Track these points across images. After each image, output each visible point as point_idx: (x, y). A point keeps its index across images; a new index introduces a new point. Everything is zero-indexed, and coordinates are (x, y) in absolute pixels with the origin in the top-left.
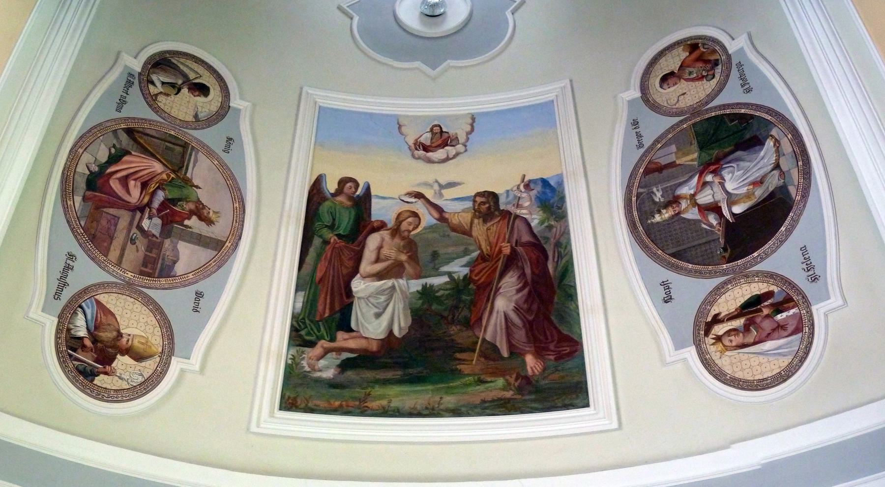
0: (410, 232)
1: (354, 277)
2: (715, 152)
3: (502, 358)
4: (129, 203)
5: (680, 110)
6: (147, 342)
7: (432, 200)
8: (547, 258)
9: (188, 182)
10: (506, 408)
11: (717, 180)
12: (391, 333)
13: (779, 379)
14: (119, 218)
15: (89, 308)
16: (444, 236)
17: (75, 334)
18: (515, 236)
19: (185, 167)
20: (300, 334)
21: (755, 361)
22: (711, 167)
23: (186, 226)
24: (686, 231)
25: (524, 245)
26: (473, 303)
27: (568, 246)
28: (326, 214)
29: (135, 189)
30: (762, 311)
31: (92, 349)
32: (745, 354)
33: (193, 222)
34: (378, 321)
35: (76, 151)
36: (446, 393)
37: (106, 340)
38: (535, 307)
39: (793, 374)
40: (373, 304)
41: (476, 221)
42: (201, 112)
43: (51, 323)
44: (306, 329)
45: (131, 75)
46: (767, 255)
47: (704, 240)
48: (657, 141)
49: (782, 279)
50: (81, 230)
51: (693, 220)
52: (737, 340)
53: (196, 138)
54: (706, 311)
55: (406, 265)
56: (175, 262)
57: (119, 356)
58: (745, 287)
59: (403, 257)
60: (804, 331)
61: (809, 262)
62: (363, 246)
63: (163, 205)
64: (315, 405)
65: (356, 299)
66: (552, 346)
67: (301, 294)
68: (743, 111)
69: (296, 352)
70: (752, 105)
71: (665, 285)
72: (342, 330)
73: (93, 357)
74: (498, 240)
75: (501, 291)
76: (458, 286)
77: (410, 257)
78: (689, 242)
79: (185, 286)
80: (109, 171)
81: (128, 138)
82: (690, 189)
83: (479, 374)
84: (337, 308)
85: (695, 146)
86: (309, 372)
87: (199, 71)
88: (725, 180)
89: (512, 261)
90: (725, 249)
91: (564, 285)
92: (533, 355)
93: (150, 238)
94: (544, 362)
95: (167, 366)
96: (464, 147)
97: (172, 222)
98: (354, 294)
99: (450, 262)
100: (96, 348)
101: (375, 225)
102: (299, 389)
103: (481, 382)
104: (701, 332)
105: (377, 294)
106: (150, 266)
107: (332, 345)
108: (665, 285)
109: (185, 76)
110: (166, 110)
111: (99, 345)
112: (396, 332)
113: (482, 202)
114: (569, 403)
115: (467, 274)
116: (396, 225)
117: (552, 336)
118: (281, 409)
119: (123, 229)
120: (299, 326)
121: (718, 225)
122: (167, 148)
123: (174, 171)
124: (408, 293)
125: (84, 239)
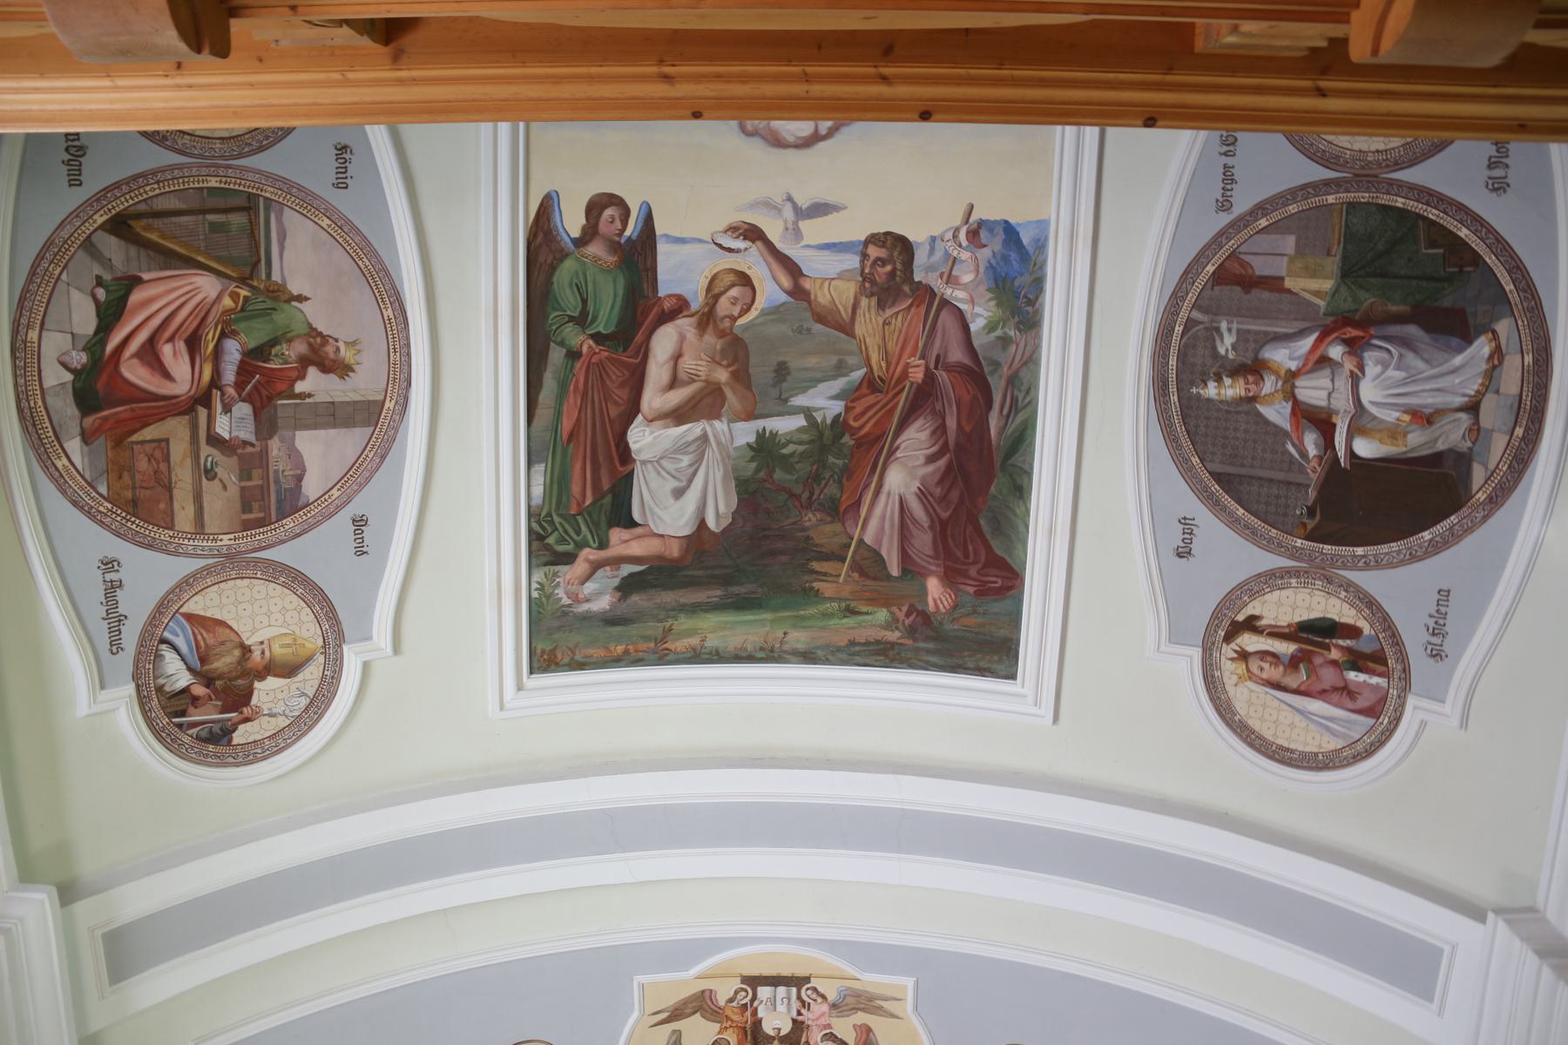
0: (735, 319)
2: (1368, 300)
3: (889, 577)
5: (1335, 150)
6: (295, 640)
7: (779, 245)
8: (989, 406)
9: (279, 295)
10: (886, 656)
11: (1349, 365)
12: (702, 524)
13: (1311, 762)
14: (167, 441)
15: (177, 635)
16: (800, 331)
17: (173, 688)
18: (936, 349)
19: (263, 262)
20: (548, 544)
21: (1287, 716)
22: (1349, 329)
23: (302, 396)
24: (1255, 441)
25: (949, 368)
26: (847, 472)
28: (568, 291)
29: (175, 357)
30: (1329, 650)
31: (210, 696)
32: (1275, 700)
33: (313, 383)
34: (679, 504)
35: (25, 342)
36: (794, 626)
37: (226, 670)
38: (955, 495)
39: (1335, 768)
40: (669, 473)
41: (864, 302)
43: (122, 697)
44: (556, 533)
46: (1378, 565)
47: (1280, 476)
48: (1261, 209)
49: (1385, 620)
50: (106, 504)
51: (1276, 426)
52: (1274, 673)
53: (268, 175)
54: (1239, 603)
57: (257, 684)
58: (1319, 597)
59: (722, 375)
60: (1380, 720)
61: (1441, 622)
63: (244, 371)
64: (586, 657)
65: (638, 462)
66: (973, 572)
67: (539, 469)
68: (1463, 233)
69: (543, 577)
70: (1491, 230)
71: (1187, 525)
72: (618, 526)
74: (903, 349)
75: (898, 454)
76: (821, 435)
78: (1252, 466)
79: (331, 515)
80: (110, 347)
81: (123, 243)
82: (1291, 359)
83: (846, 600)
84: (606, 485)
85: (1333, 264)
86: (569, 606)
88: (1364, 374)
89: (924, 398)
90: (1311, 512)
91: (1014, 465)
92: (939, 577)
93: (240, 451)
94: (955, 594)
95: (338, 663)
97: (270, 399)
98: (633, 455)
100: (215, 691)
101: (667, 305)
102: (556, 636)
103: (852, 612)
104: (1220, 631)
106: (255, 506)
107: (603, 554)
108: (1187, 525)
111: (218, 683)
112: (711, 523)
113: (878, 259)
114: (986, 666)
115: (840, 414)
116: (707, 304)
117: (976, 553)
119: (183, 460)
121: (1316, 460)
122: (215, 227)
123: (243, 281)
124: (731, 450)
125: (119, 519)
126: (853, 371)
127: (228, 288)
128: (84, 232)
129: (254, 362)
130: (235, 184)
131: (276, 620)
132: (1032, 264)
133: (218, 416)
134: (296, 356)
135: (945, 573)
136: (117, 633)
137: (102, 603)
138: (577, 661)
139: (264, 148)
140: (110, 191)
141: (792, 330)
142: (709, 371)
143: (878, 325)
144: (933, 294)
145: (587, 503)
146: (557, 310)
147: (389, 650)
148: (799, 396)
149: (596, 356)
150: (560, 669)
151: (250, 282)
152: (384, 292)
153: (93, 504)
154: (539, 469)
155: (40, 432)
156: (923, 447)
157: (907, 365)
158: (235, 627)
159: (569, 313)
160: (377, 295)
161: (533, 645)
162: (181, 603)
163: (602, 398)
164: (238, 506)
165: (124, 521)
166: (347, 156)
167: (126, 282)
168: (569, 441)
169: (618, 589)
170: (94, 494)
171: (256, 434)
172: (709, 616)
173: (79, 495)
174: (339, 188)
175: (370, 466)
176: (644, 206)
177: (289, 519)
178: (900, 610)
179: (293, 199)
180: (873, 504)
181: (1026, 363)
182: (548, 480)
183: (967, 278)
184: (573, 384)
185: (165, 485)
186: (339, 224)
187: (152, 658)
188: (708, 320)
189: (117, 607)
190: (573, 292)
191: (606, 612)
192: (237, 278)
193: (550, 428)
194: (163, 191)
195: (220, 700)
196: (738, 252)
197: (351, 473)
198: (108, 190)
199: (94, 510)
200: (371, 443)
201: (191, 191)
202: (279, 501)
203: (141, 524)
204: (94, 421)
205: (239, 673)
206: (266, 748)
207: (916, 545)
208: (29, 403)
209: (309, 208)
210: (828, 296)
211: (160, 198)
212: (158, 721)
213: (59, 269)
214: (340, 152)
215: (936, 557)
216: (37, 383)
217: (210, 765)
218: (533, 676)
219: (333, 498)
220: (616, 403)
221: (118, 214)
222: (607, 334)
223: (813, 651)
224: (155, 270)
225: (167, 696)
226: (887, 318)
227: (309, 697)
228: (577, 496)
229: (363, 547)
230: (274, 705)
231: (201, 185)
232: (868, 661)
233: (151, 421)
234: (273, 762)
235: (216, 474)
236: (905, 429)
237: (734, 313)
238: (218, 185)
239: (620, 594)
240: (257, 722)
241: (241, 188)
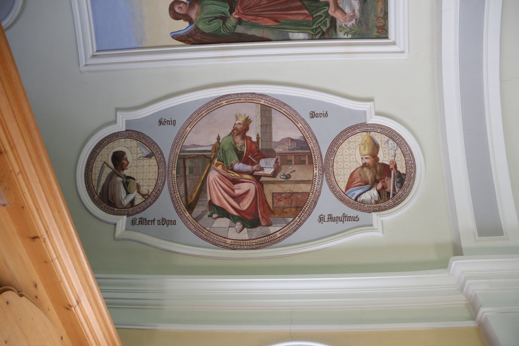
4: (256, 189)
6: (362, 144)
9: (217, 147)
14: (273, 193)
17: (377, 197)
20: (326, 31)
23: (258, 138)
28: (212, 26)
29: (243, 188)
31: (383, 182)
33: (253, 134)
35: (231, 245)
37: (372, 174)
42: (143, 153)
45: (133, 222)
50: (296, 219)
53: (171, 151)
56: (292, 140)
57: (380, 162)
63: (247, 162)
64: (382, 11)
67: (291, 35)
69: (342, 32)
73: (387, 180)
79: (309, 127)
80: (235, 213)
81: (197, 207)
84: (299, 4)
86: (356, 20)
87: (100, 166)
93: (279, 165)
95: (375, 126)
97: (259, 151)
100: (381, 179)
102: (370, 26)
106: (303, 159)
109: (110, 177)
110: (154, 183)
111: (377, 178)
118: (387, 38)
122: (191, 172)
123: (211, 161)
125: (303, 214)
127: (214, 167)
128: (192, 221)
129: (243, 158)
130: (175, 164)
131: (353, 152)
133: (264, 173)
134: (242, 141)
136: (350, 218)
137: (337, 223)
139: (161, 153)
140: (178, 210)
146: (220, 30)
147: (371, 103)
150: (387, 24)
151: (212, 159)
152: (216, 104)
153: (296, 224)
155: (265, 242)
158: (354, 169)
159: (221, 25)
160: (217, 107)
162: (341, 191)
163: (258, 7)
164: (302, 166)
165: (304, 212)
166: (163, 120)
167: (211, 206)
170: (292, 223)
171: (273, 158)
173: (292, 229)
174: (175, 124)
175: (288, 110)
177: (309, 145)
179: (180, 142)
182: (297, 31)
185: (291, 195)
186: (189, 123)
187: (363, 204)
189: (339, 217)
190: (212, 23)
192: (210, 163)
193: (273, 31)
194: (178, 191)
195: (385, 177)
197: (291, 118)
198: (177, 211)
199: (298, 223)
200: (278, 110)
201: (177, 181)
202: (302, 149)
203: (306, 205)
204: (263, 221)
205: (374, 169)
206: (409, 159)
208: (254, 245)
209: (183, 135)
211: (180, 192)
212: (390, 204)
213: (205, 230)
214: (162, 123)
216: (247, 241)
217: (413, 184)
218: (389, 37)
219: (301, 126)
221: (186, 208)
222: (230, 6)
224: (207, 195)
225: (380, 199)
227: (389, 139)
228: (304, 17)
229: (324, 114)
230: (391, 155)
231: (175, 177)
233: (265, 200)
234: (416, 157)
235: (288, 174)
238: (175, 171)
240: (397, 163)
241: (176, 161)
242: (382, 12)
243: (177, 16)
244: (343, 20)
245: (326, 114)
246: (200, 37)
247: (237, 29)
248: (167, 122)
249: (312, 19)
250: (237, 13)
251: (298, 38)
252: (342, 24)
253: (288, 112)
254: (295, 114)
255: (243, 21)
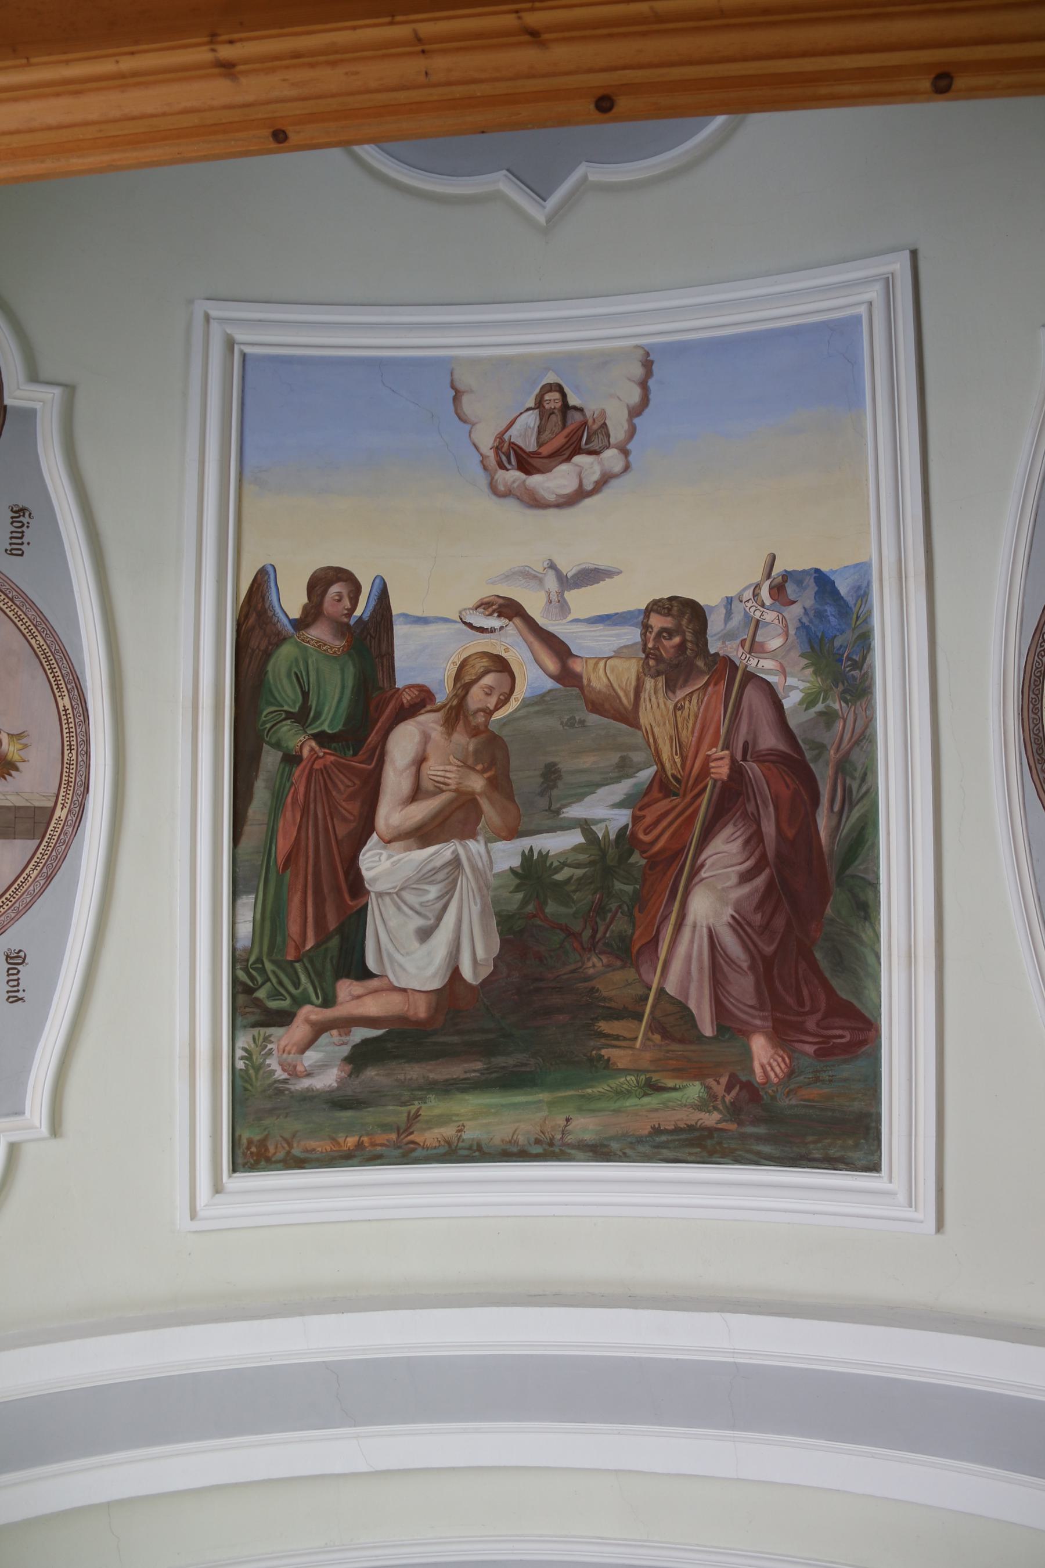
0: (491, 713)
1: (365, 844)
3: (700, 1038)
8: (815, 801)
12: (455, 974)
16: (571, 723)
20: (257, 999)
25: (761, 758)
26: (640, 901)
27: (869, 774)
28: (285, 681)
34: (426, 947)
36: (580, 1110)
38: (779, 922)
40: (412, 908)
41: (649, 684)
44: (269, 984)
55: (485, 804)
59: (477, 783)
62: (379, 757)
64: (307, 1151)
65: (373, 895)
66: (811, 1024)
67: (247, 902)
69: (251, 1042)
72: (348, 976)
75: (703, 874)
77: (493, 783)
84: (332, 924)
86: (285, 1081)
91: (853, 877)
92: (766, 1034)
94: (789, 1058)
96: (621, 457)
98: (367, 886)
99: (586, 794)
101: (406, 698)
102: (266, 1122)
103: (656, 1088)
105: (419, 881)
112: (467, 972)
113: (663, 630)
114: (838, 1154)
115: (627, 825)
118: (234, 1169)
120: (252, 978)
124: (490, 877)
126: (641, 770)
132: (855, 617)
135: (774, 1028)
138: (294, 1156)
141: (562, 723)
142: (460, 778)
143: (668, 710)
144: (734, 667)
145: (308, 947)
146: (272, 704)
147: (44, 1130)
148: (574, 805)
149: (321, 761)
150: (273, 1166)
152: (60, 678)
154: (247, 902)
156: (734, 861)
157: (708, 759)
159: (286, 708)
160: (52, 680)
161: (237, 1134)
166: (25, 520)
168: (286, 867)
169: (349, 1059)
172: (467, 1097)
175: (32, 888)
176: (378, 581)
178: (718, 1083)
180: (674, 942)
181: (858, 742)
182: (258, 916)
183: (775, 643)
184: (290, 795)
186: (10, 596)
188: (457, 715)
190: (291, 682)
191: (331, 1091)
193: (262, 850)
196: (491, 632)
200: (35, 859)
207: (734, 994)
210: (605, 680)
214: (17, 515)
215: (761, 1007)
218: (237, 1174)
220: (344, 819)
222: (334, 734)
223: (606, 1143)
226: (678, 702)
229: (18, 991)
232: (679, 1155)
236: (710, 841)
237: (489, 705)
239: (351, 1066)
242: (304, 1152)
243: (317, 588)
244: (286, 1046)
245: (16, 997)
246: (255, 647)
247: (273, 751)
248: (20, 530)
249: (289, 958)
250: (316, 753)
251: (239, 921)
252: (273, 1042)
253: (26, 887)
254: (21, 908)
255: (294, 769)
